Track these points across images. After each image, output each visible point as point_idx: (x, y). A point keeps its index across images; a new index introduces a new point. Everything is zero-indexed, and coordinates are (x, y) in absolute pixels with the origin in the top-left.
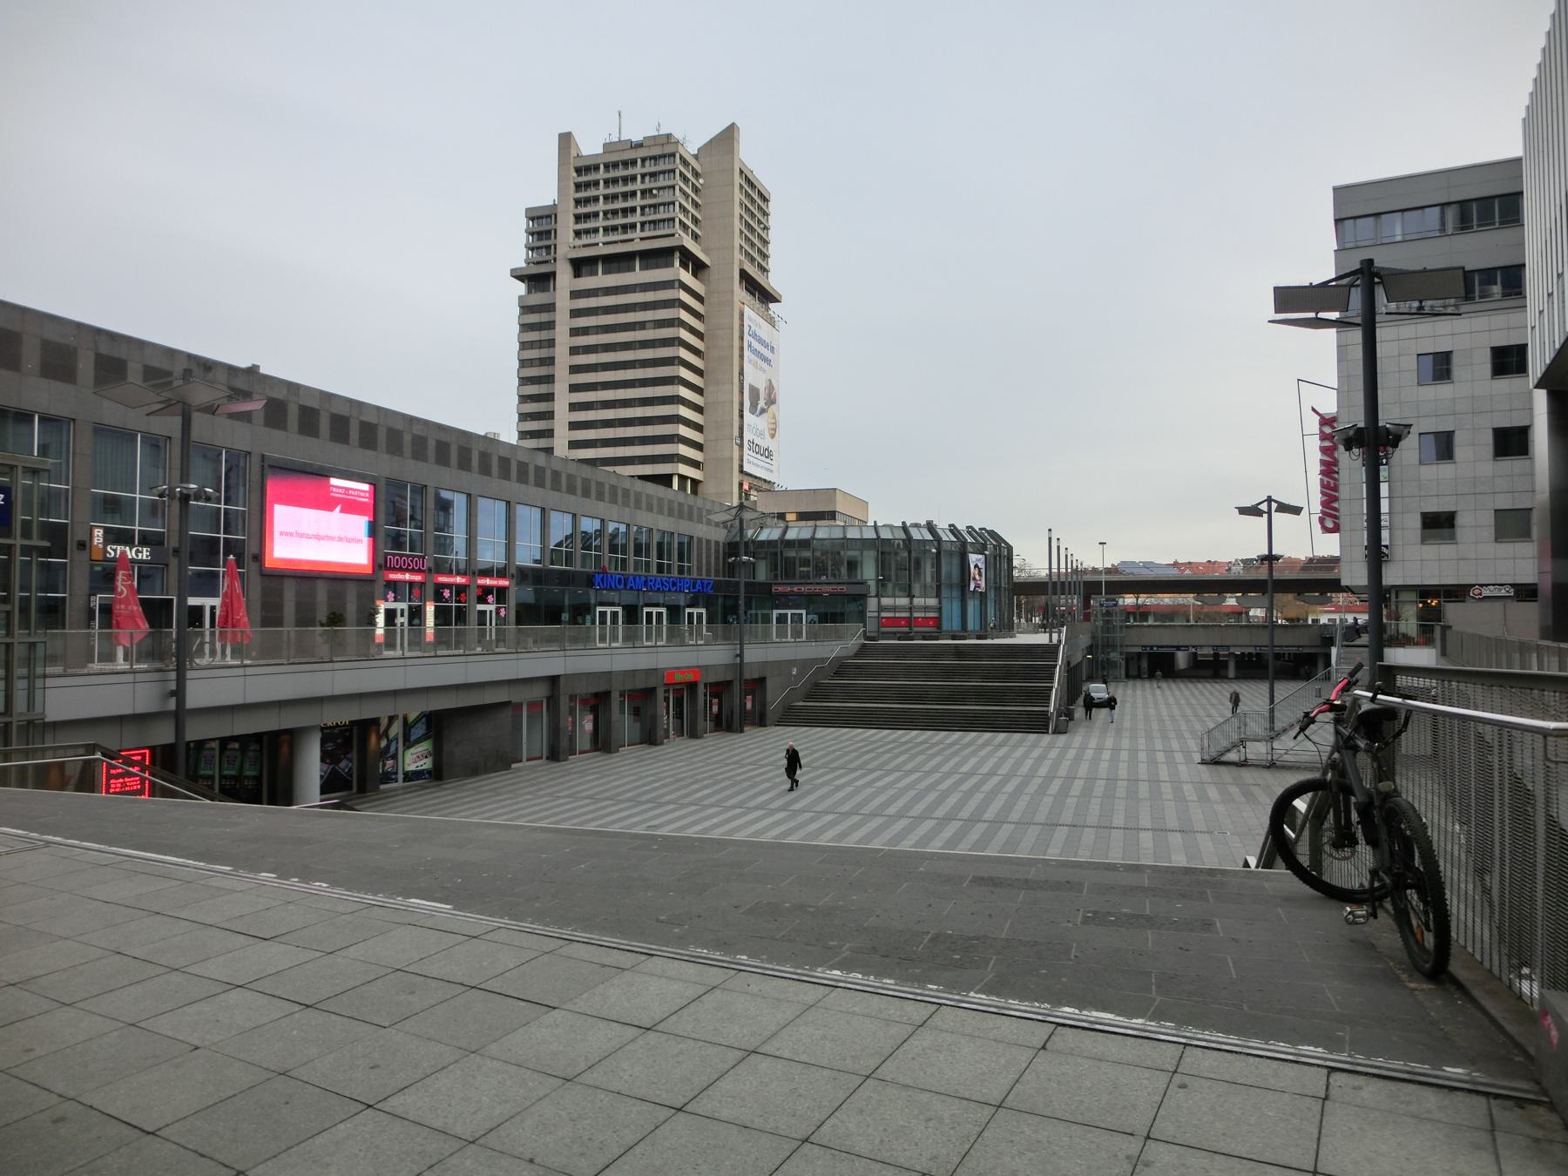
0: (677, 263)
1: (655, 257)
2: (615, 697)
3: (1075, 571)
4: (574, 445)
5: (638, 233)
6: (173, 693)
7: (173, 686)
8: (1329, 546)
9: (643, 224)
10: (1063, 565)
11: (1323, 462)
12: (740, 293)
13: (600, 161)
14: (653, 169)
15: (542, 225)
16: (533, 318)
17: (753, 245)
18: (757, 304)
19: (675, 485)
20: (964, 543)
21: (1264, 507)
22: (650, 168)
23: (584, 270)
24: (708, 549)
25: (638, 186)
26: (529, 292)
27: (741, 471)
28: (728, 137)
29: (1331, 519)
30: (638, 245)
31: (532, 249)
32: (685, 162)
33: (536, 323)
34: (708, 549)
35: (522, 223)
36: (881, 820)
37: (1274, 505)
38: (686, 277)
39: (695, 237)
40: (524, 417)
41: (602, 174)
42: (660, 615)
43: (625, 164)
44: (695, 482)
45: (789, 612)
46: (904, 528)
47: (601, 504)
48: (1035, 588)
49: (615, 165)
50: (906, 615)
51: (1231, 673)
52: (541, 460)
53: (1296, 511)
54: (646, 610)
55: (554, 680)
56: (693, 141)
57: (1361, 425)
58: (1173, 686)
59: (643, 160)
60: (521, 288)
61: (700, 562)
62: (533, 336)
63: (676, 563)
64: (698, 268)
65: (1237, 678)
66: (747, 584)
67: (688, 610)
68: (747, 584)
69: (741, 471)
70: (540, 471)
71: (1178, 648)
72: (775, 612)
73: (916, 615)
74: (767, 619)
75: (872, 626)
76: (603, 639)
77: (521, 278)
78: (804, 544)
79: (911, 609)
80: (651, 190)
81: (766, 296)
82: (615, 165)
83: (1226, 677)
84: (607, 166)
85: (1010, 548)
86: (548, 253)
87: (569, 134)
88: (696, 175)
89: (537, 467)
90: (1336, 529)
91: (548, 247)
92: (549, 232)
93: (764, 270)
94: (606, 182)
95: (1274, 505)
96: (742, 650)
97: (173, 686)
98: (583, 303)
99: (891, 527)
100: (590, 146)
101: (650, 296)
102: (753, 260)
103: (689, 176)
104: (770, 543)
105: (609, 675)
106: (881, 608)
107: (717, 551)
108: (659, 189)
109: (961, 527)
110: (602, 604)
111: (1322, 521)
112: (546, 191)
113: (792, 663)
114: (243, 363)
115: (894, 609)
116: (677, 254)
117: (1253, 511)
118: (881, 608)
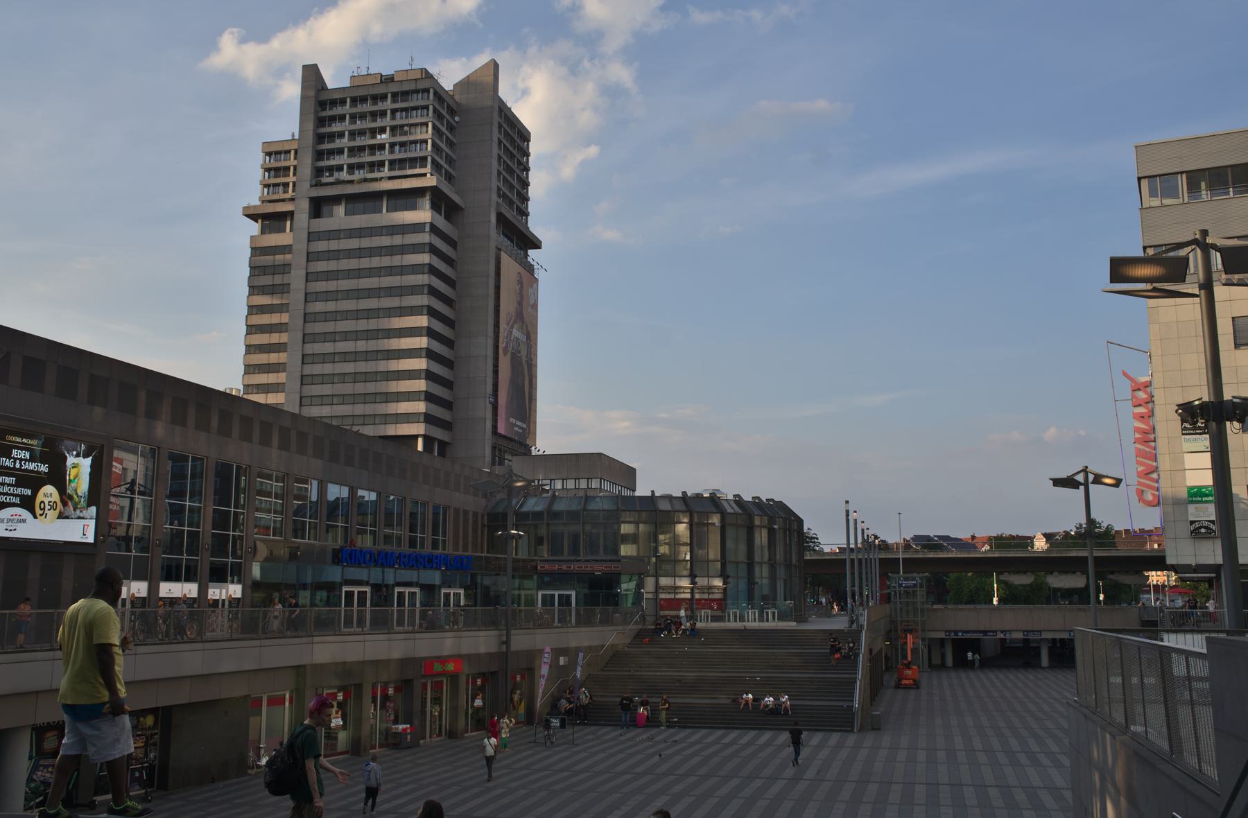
0: (427, 204)
3: (868, 545)
6: (503, 643)
7: (504, 639)
9: (394, 112)
10: (860, 540)
12: (495, 237)
13: (347, 95)
18: (516, 251)
21: (1080, 478)
23: (325, 209)
24: (466, 521)
26: (263, 232)
31: (267, 186)
36: (672, 777)
37: (1091, 477)
41: (347, 109)
42: (362, 595)
44: (443, 445)
45: (557, 593)
49: (363, 99)
51: (1045, 661)
54: (397, 590)
57: (1206, 399)
58: (992, 676)
60: (254, 228)
63: (429, 537)
65: (1051, 667)
67: (444, 591)
71: (985, 632)
76: (400, 623)
77: (253, 217)
80: (402, 126)
82: (363, 99)
87: (315, 67)
88: (452, 112)
94: (393, 129)
95: (1091, 477)
96: (508, 635)
97: (504, 639)
103: (444, 113)
107: (475, 522)
110: (399, 584)
111: (1140, 493)
114: (221, 389)
117: (1067, 482)
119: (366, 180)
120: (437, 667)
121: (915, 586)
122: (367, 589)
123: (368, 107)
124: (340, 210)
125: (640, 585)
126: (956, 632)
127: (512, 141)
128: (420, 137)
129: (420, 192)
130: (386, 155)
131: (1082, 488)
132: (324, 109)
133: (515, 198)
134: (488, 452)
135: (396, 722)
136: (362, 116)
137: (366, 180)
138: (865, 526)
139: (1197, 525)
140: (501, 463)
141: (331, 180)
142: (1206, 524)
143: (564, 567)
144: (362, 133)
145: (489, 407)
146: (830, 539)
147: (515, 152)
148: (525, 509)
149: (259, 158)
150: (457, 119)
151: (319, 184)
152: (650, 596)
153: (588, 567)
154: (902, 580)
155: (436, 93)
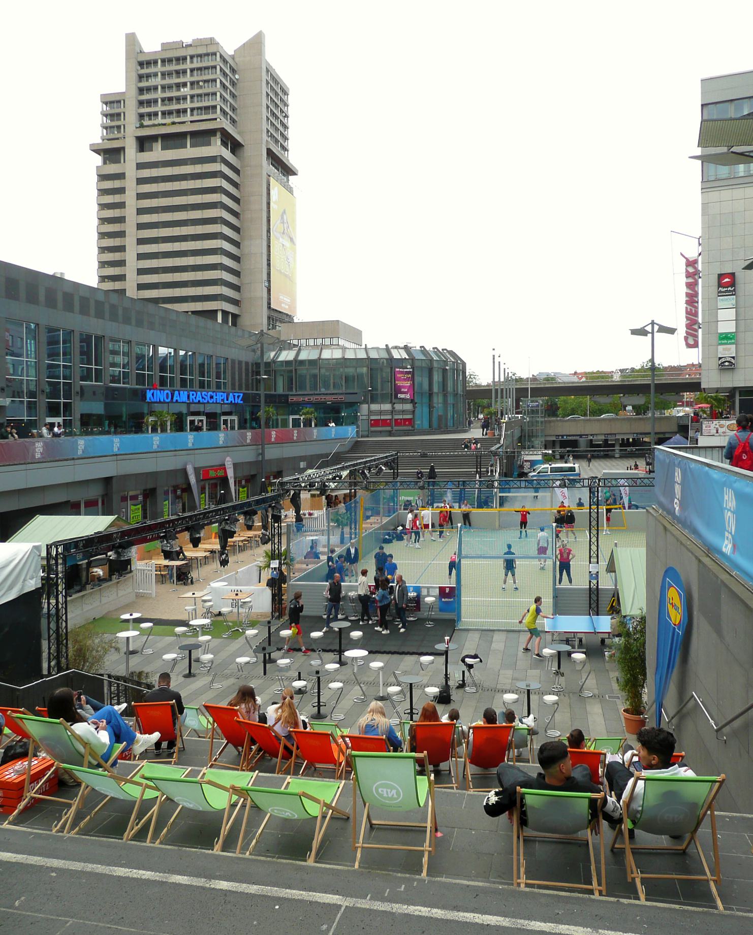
0: (219, 142)
1: (202, 137)
2: (160, 492)
4: (141, 287)
5: (188, 117)
6: (259, 454)
8: (693, 357)
9: (192, 110)
11: (687, 294)
12: (267, 167)
13: (158, 57)
14: (200, 65)
15: (113, 107)
16: (108, 185)
17: (277, 129)
19: (220, 320)
20: (431, 360)
21: (649, 328)
22: (196, 64)
23: (147, 145)
25: (188, 78)
26: (105, 163)
27: (269, 308)
28: (256, 44)
29: (691, 341)
30: (193, 132)
32: (225, 61)
33: (110, 187)
34: (233, 368)
35: (99, 107)
38: (227, 154)
39: (233, 121)
40: (103, 264)
41: (159, 68)
43: (178, 59)
44: (235, 317)
46: (388, 350)
47: (152, 332)
48: (484, 393)
49: (170, 60)
50: (389, 417)
52: (114, 299)
53: (671, 331)
55: (107, 481)
56: (229, 46)
59: (192, 57)
60: (98, 160)
61: (233, 378)
62: (109, 199)
64: (235, 146)
66: (266, 395)
68: (266, 395)
69: (269, 308)
70: (113, 307)
71: (581, 436)
72: (291, 417)
73: (396, 417)
74: (285, 423)
75: (363, 425)
77: (97, 151)
78: (312, 363)
79: (393, 412)
80: (198, 82)
81: (287, 170)
83: (613, 457)
84: (163, 61)
85: (464, 364)
86: (119, 132)
88: (233, 71)
89: (97, 302)
90: (695, 345)
91: (119, 127)
92: (119, 115)
93: (285, 149)
95: (656, 328)
98: (146, 173)
99: (378, 349)
100: (151, 45)
101: (198, 168)
102: (277, 141)
104: (288, 363)
105: (154, 475)
106: (370, 412)
107: (247, 370)
108: (205, 81)
109: (429, 348)
111: (686, 339)
112: (117, 80)
113: (302, 458)
114: (51, 273)
115: (381, 412)
116: (219, 135)
117: (641, 332)
118: (370, 412)
119: (173, 123)
120: (212, 474)
121: (538, 406)
122: (204, 418)
123: (174, 67)
124: (158, 146)
125: (57, 551)
126: (562, 436)
127: (277, 94)
128: (210, 90)
129: (212, 132)
130: (188, 105)
131: (650, 335)
132: (142, 68)
133: (279, 138)
134: (265, 321)
135: (184, 511)
136: (170, 74)
137: (173, 123)
138: (505, 367)
139: (723, 360)
140: (274, 327)
141: (150, 123)
142: (729, 359)
143: (306, 399)
144: (170, 87)
145: (265, 290)
146: (481, 374)
147: (279, 103)
148: (279, 359)
149: (99, 107)
150: (237, 76)
151: (142, 126)
152: (364, 418)
153: (322, 398)
154: (529, 403)
155: (221, 56)
